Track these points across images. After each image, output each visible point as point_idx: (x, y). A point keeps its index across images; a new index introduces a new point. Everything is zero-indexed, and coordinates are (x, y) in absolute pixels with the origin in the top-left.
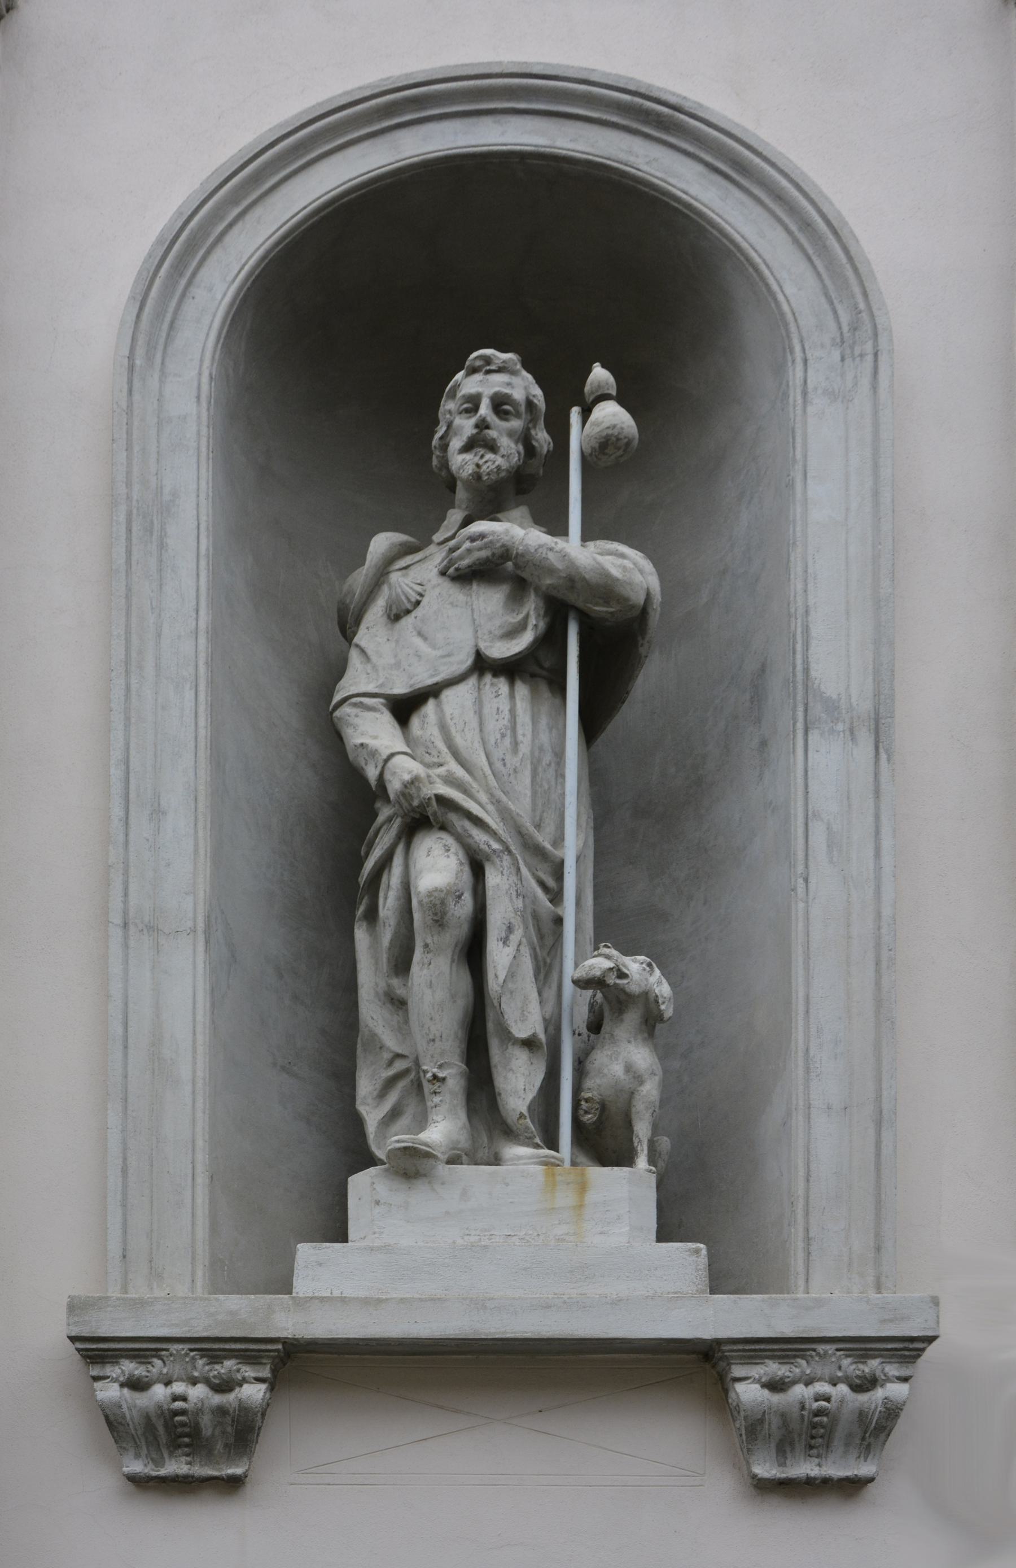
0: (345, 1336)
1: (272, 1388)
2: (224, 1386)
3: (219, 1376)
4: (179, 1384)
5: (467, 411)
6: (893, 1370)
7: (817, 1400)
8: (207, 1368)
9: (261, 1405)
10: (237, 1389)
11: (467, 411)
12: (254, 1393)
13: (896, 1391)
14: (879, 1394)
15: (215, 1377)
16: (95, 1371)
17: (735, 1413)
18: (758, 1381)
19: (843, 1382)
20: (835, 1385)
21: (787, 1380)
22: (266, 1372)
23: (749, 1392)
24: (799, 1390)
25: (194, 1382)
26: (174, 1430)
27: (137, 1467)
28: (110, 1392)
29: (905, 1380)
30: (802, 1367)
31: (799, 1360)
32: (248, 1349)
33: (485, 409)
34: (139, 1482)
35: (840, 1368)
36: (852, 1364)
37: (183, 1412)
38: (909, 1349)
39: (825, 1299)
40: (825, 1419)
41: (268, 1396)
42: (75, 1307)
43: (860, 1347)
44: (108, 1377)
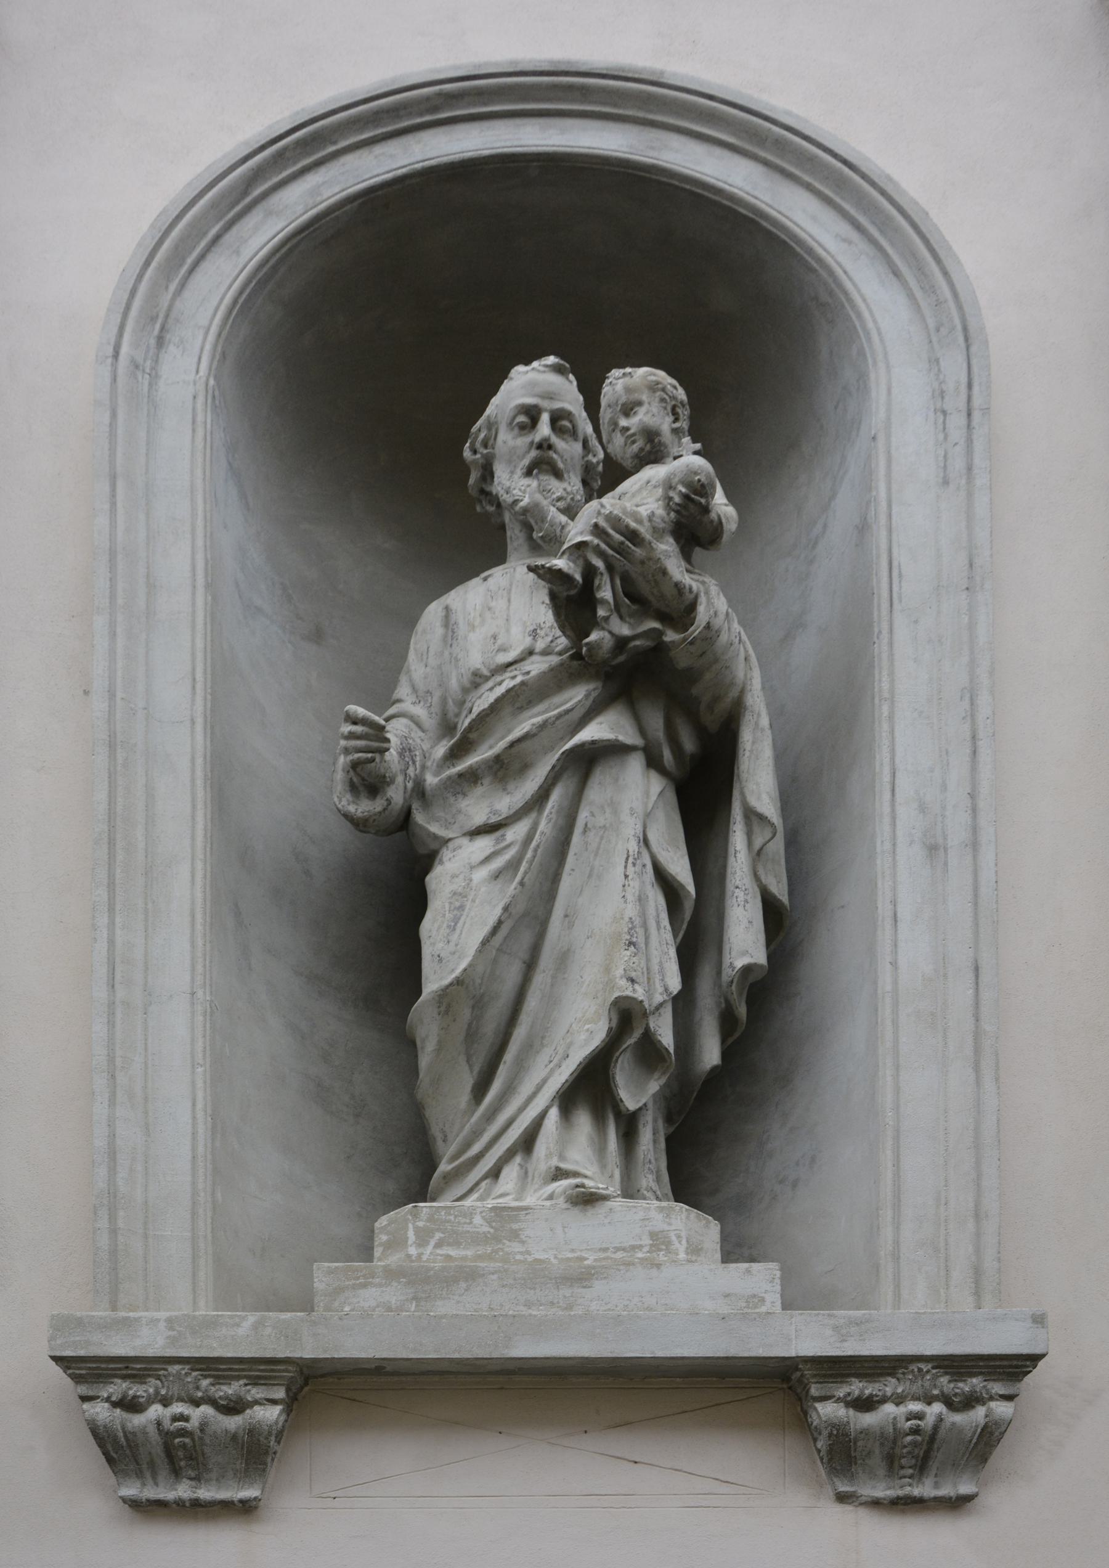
0: (610, 1355)
1: (289, 1409)
2: (233, 1407)
3: (227, 1398)
4: (180, 1404)
5: (522, 427)
6: (998, 1388)
7: (908, 1419)
8: (952, 1385)
9: (276, 1423)
10: (248, 1411)
11: (522, 427)
12: (270, 1414)
13: (1002, 1409)
14: (979, 1414)
15: (220, 1398)
16: (83, 1390)
17: (815, 1434)
18: (108, 1400)
19: (939, 1400)
20: (929, 1404)
21: (875, 1399)
22: (280, 1393)
23: (828, 1411)
24: (155, 1411)
25: (196, 1403)
26: (181, 1453)
27: (131, 1490)
28: (101, 1411)
29: (1009, 1398)
30: (890, 1386)
31: (890, 1379)
32: (259, 1369)
33: (544, 429)
34: (135, 1504)
35: (198, 1388)
36: (950, 1382)
37: (183, 1433)
38: (1014, 1367)
39: (911, 1319)
40: (187, 1440)
41: (283, 1418)
42: (61, 1324)
43: (957, 1365)
44: (98, 1397)
